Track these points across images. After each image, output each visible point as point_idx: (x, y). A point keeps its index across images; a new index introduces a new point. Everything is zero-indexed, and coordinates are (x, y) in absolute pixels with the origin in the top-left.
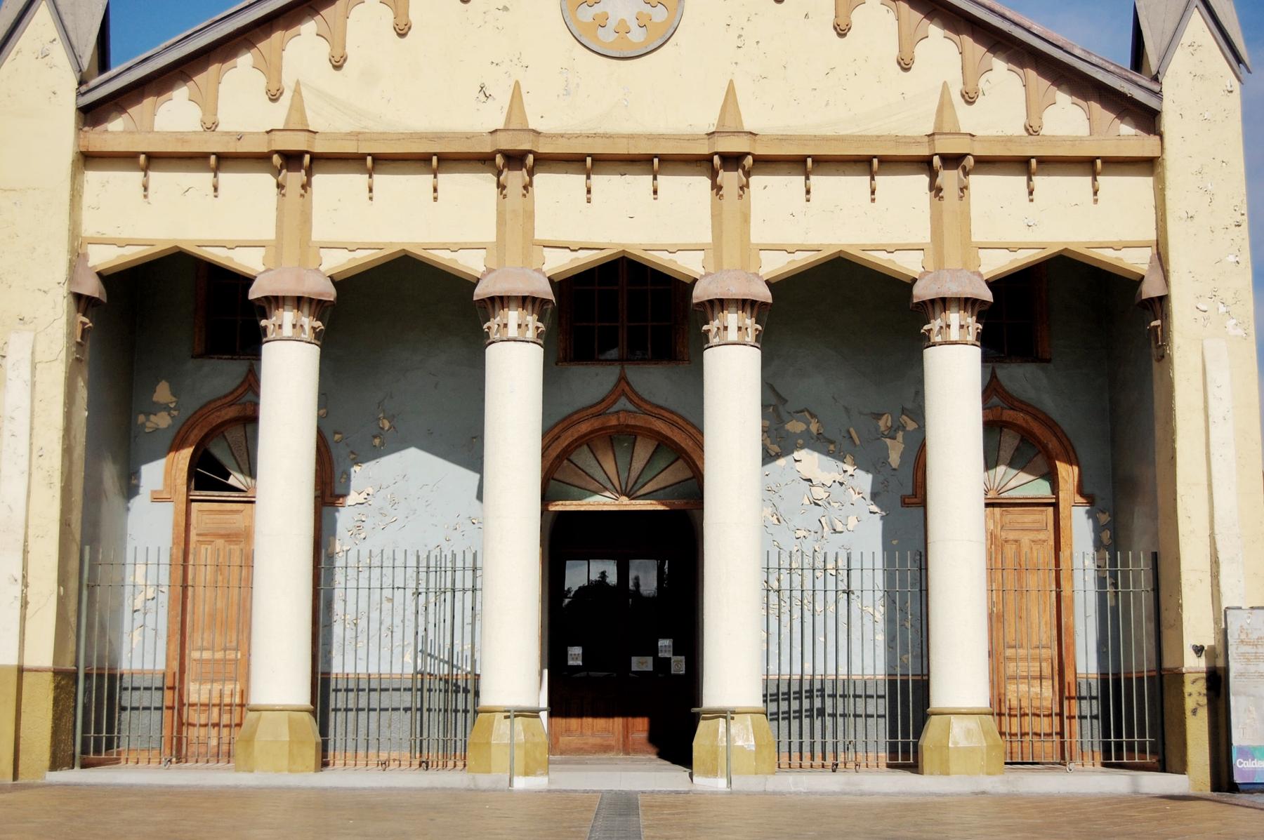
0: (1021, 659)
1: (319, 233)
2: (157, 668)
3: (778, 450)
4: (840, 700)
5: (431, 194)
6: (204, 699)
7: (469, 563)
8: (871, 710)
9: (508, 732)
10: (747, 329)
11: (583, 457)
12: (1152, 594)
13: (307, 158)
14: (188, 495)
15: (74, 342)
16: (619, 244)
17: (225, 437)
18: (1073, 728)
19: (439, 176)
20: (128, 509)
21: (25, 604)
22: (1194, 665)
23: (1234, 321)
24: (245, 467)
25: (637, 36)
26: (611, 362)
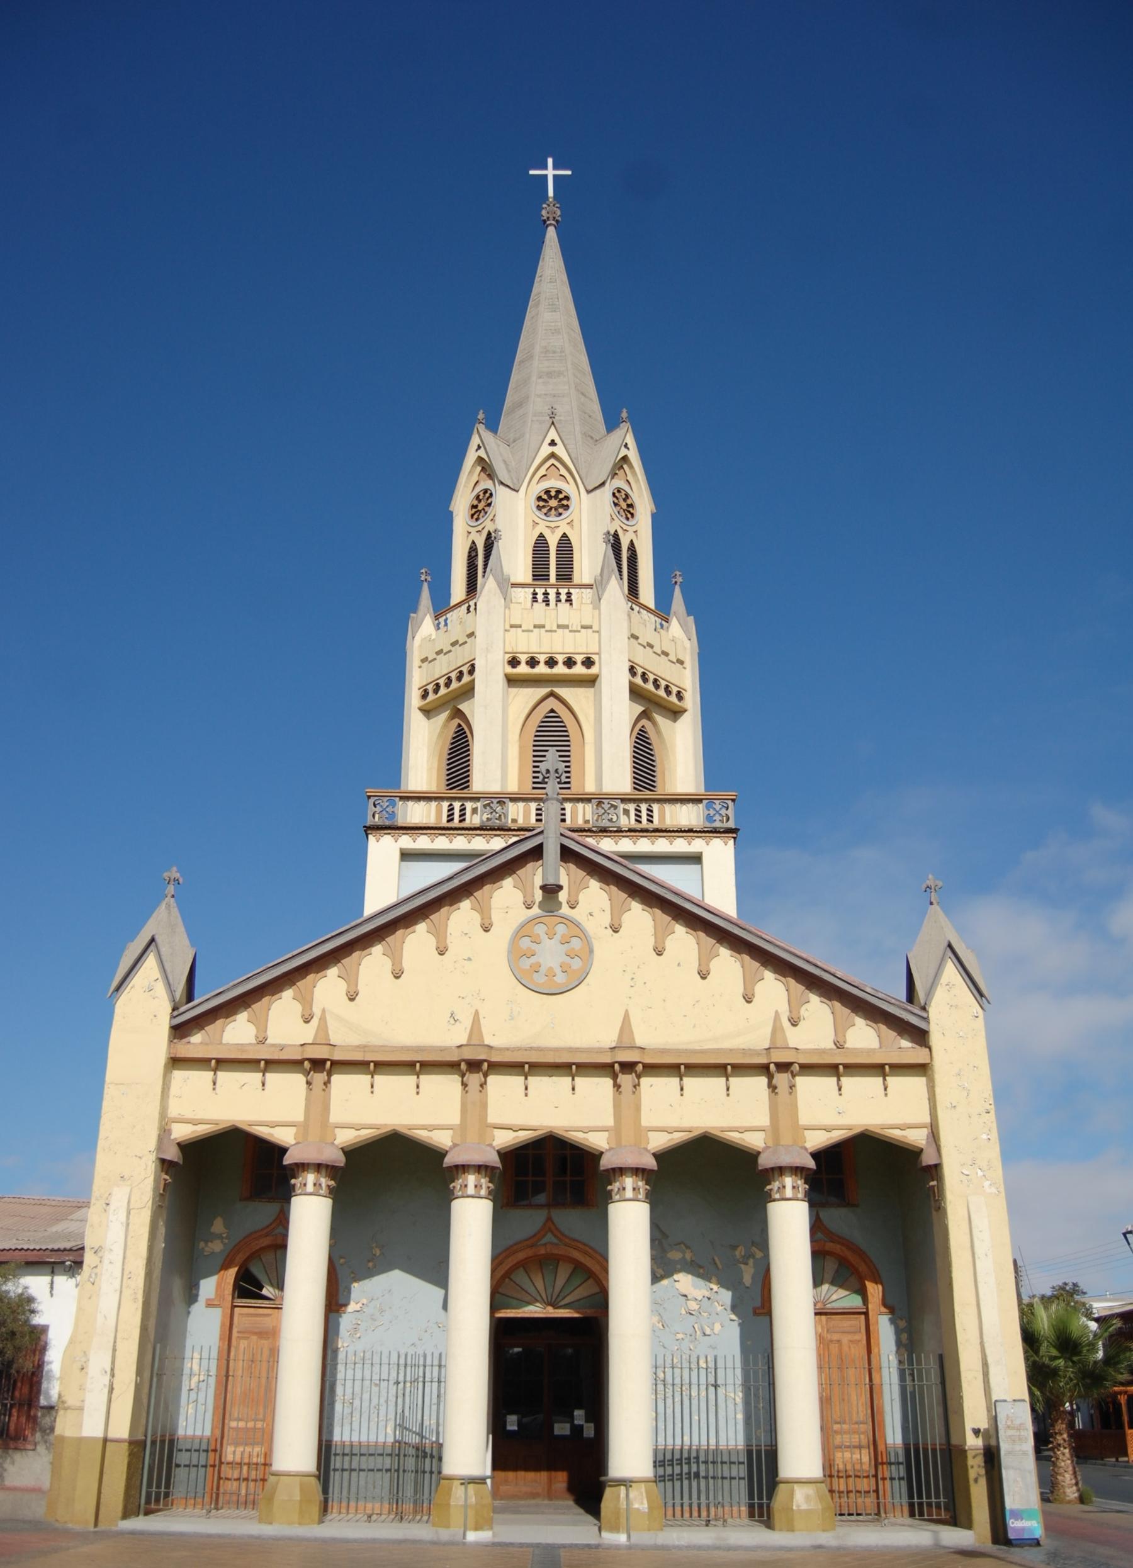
0: (845, 1433)
1: (335, 1117)
2: (205, 1434)
3: (663, 1273)
4: (711, 1466)
5: (415, 1090)
6: (238, 1459)
7: (436, 1362)
8: (734, 1474)
9: (463, 1496)
10: (639, 1189)
11: (520, 1277)
12: (940, 1386)
13: (328, 1064)
14: (232, 1302)
15: (158, 1194)
16: (547, 1127)
17: (260, 1258)
18: (886, 1486)
19: (421, 1076)
20: (189, 1313)
21: (111, 1390)
22: (973, 1442)
23: (989, 1182)
24: (274, 1282)
25: (560, 978)
26: (540, 1206)
